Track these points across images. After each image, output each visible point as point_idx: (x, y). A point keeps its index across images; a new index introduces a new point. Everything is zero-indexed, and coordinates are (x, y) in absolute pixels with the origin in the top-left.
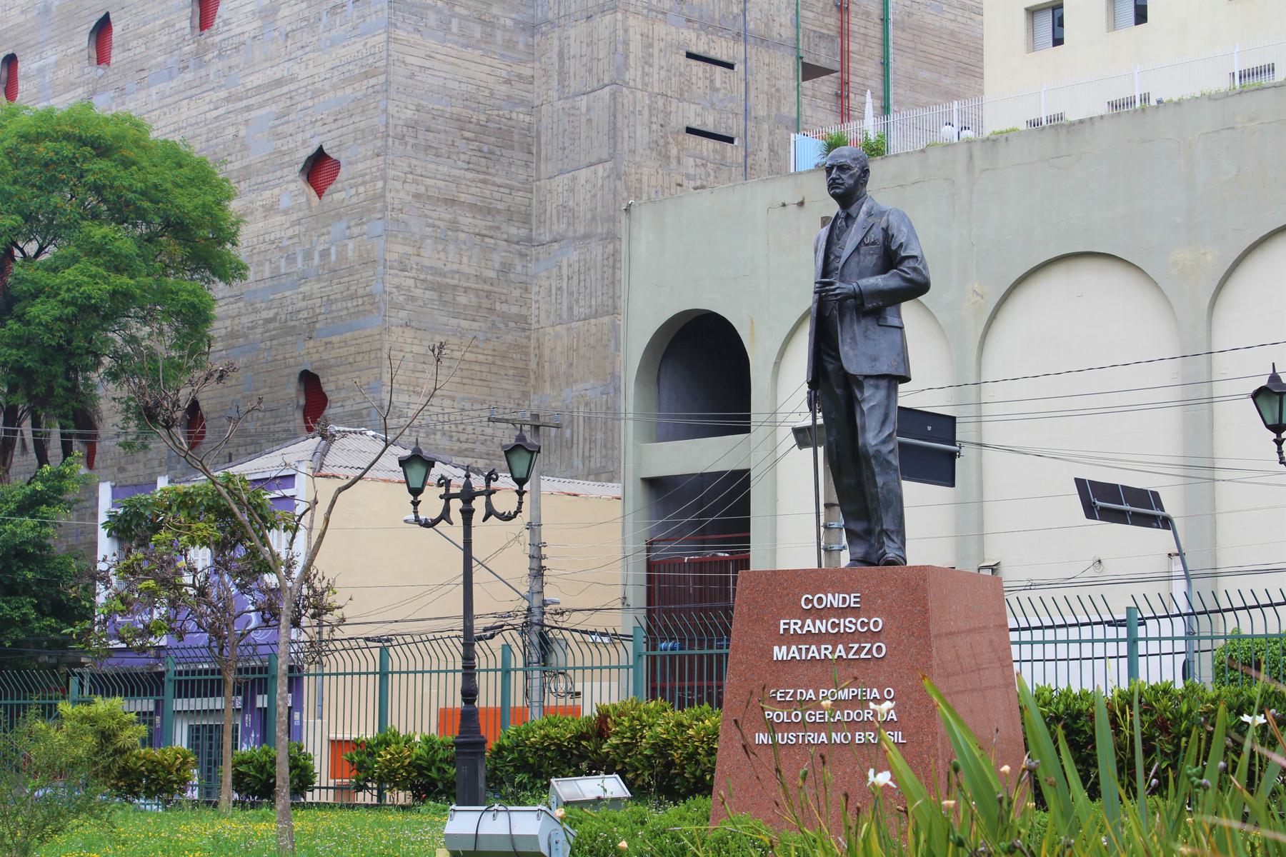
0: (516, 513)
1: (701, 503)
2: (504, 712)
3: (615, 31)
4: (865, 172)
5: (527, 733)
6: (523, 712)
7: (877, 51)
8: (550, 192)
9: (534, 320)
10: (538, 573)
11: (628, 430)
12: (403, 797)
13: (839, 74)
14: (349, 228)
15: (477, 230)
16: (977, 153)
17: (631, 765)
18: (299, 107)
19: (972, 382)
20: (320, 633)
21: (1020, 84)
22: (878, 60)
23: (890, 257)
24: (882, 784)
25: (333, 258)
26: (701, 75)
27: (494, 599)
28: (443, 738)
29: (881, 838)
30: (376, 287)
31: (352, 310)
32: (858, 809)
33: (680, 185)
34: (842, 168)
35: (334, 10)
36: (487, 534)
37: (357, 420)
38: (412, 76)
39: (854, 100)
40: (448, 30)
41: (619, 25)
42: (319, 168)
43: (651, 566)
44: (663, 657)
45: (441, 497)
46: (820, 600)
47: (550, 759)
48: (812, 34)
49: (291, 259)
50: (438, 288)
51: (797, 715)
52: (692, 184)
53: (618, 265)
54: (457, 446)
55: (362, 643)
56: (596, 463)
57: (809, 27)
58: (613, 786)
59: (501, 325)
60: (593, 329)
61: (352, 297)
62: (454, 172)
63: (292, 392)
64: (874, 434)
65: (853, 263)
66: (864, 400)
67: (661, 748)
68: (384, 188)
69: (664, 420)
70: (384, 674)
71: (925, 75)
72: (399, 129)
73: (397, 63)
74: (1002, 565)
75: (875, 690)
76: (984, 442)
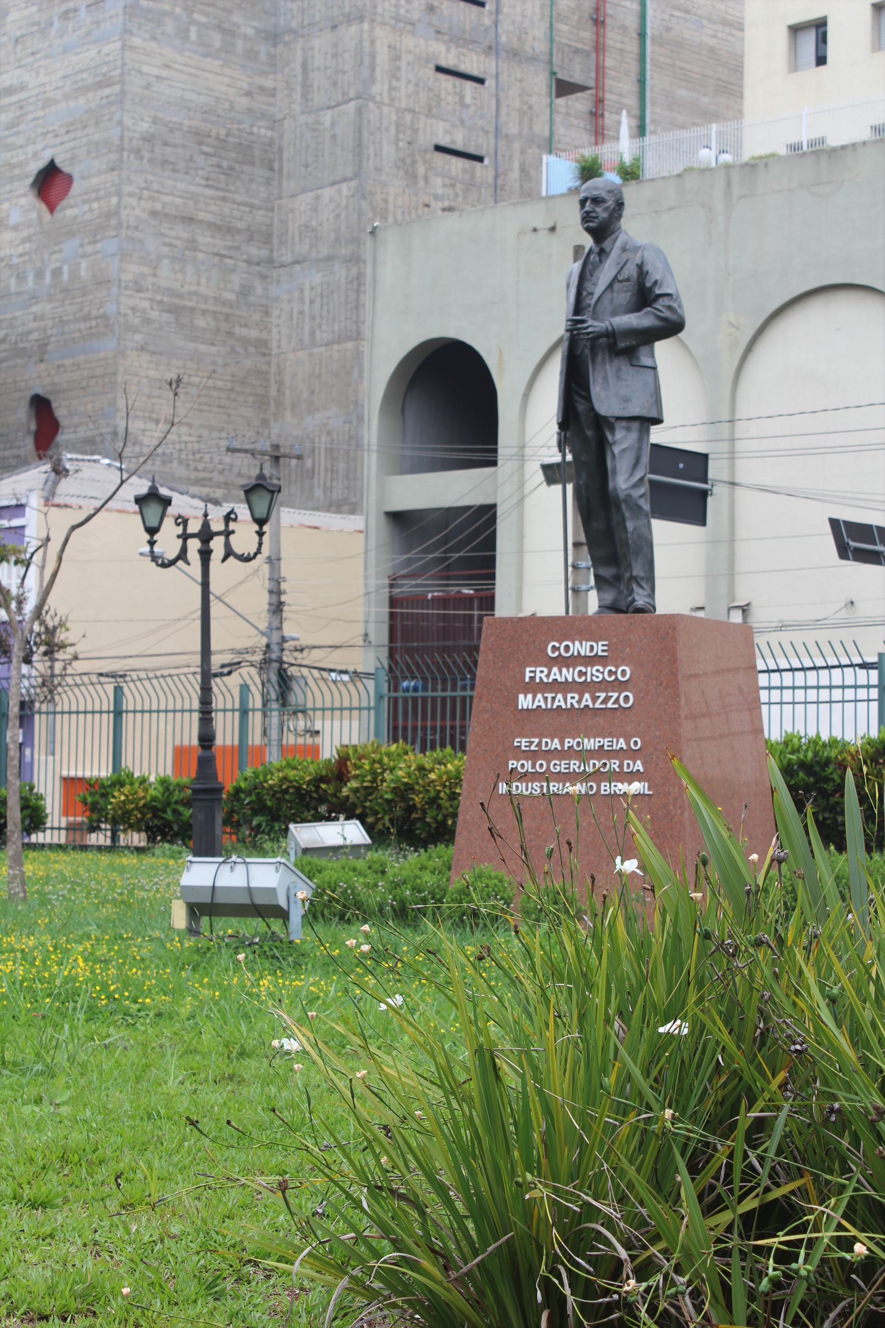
0: (256, 554)
1: (445, 540)
2: (242, 749)
3: (361, 42)
4: (620, 205)
5: (265, 776)
6: (260, 750)
7: (634, 67)
8: (292, 211)
9: (274, 345)
10: (277, 608)
11: (371, 462)
12: (137, 839)
13: (593, 92)
14: (82, 246)
15: (216, 250)
16: (736, 177)
17: (371, 809)
18: (30, 117)
19: (727, 420)
20: (52, 667)
21: (780, 109)
22: (634, 76)
23: (644, 295)
24: (629, 872)
25: (65, 277)
26: (450, 90)
27: (233, 635)
28: (179, 780)
29: (628, 920)
30: (110, 309)
31: (85, 332)
32: (605, 897)
33: (427, 206)
34: (596, 201)
35: (66, 15)
36: (222, 573)
37: (90, 446)
38: (148, 86)
39: (609, 118)
40: (186, 38)
41: (366, 36)
42: (50, 182)
43: (393, 602)
44: (405, 700)
45: (179, 537)
46: (567, 648)
47: (289, 802)
48: (566, 49)
49: (21, 278)
50: (173, 309)
51: (541, 765)
52: (440, 205)
53: (362, 289)
54: (194, 475)
55: (94, 679)
56: (338, 493)
57: (564, 41)
58: (353, 832)
59: (240, 350)
60: (336, 356)
61: (87, 318)
62: (193, 188)
63: (23, 415)
64: (626, 478)
65: (606, 301)
66: (615, 443)
67: (403, 791)
68: (119, 204)
69: (409, 453)
70: (118, 713)
71: (682, 93)
72: (135, 143)
73: (133, 73)
74: (753, 605)
75: (622, 740)
76: (737, 481)
